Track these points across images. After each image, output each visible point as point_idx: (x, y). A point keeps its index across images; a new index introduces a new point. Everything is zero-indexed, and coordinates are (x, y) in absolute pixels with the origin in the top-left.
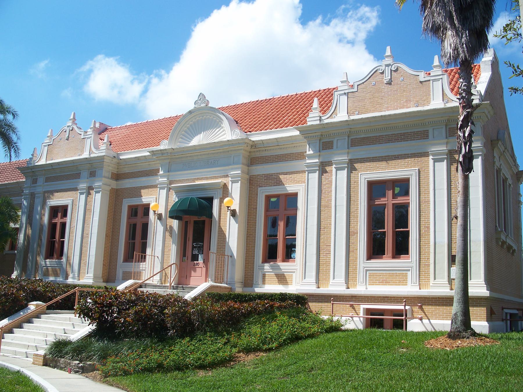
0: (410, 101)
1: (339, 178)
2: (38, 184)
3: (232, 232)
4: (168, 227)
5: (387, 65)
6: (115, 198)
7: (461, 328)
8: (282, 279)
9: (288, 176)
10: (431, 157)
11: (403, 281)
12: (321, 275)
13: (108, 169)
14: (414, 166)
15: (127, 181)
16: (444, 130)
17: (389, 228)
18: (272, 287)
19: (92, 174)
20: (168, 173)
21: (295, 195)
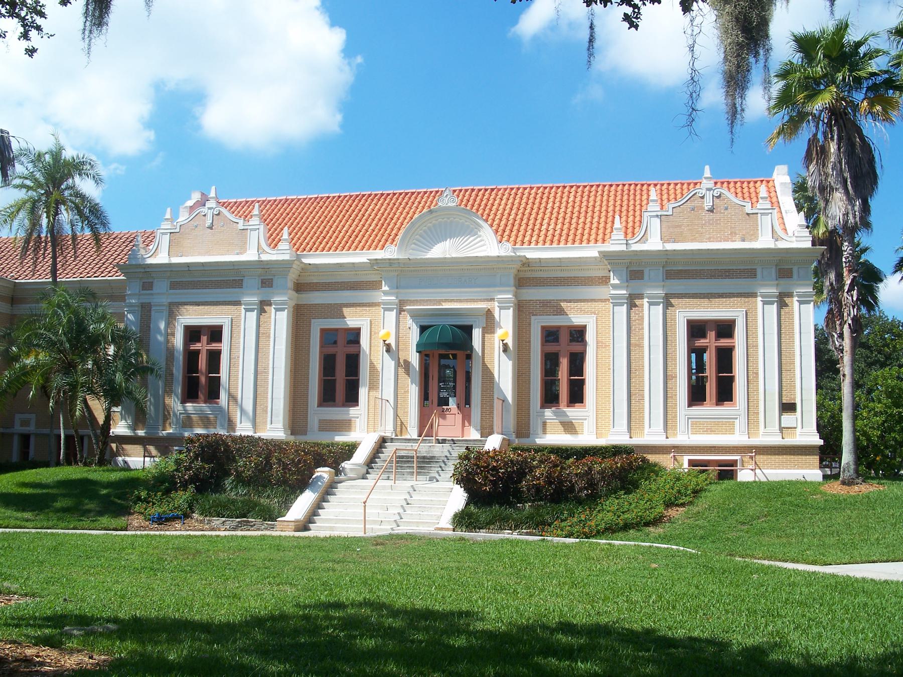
0: (735, 234)
1: (652, 315)
2: (155, 291)
3: (504, 372)
4: (401, 361)
5: (709, 189)
6: (301, 319)
7: (854, 476)
8: (569, 427)
9: (572, 305)
10: (759, 299)
11: (731, 430)
12: (633, 424)
13: (292, 276)
14: (741, 307)
15: (317, 294)
16: (773, 271)
17: (710, 371)
18: (555, 437)
19: (267, 283)
20: (396, 291)
21: (357, 332)
